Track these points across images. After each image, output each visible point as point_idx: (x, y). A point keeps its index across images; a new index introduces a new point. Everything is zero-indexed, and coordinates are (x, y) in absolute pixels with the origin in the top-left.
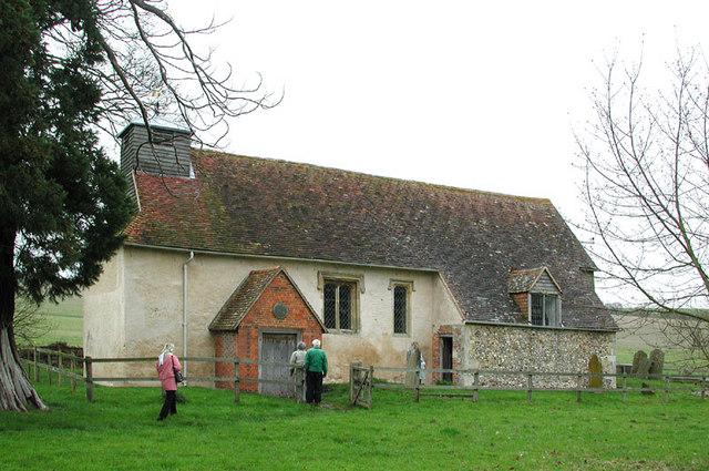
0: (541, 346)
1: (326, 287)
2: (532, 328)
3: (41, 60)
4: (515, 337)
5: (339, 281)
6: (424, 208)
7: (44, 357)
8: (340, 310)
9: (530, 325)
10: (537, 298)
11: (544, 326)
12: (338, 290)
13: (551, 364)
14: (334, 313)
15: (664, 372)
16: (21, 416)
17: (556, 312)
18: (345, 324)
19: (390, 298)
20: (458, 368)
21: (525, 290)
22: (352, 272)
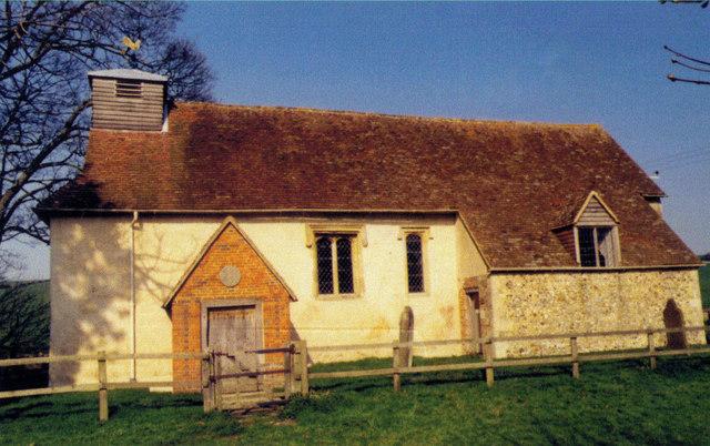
0: (596, 293)
1: (319, 243)
2: (583, 272)
3: (100, 248)
4: (563, 283)
5: (334, 234)
6: (447, 144)
7: (596, 371)
8: (335, 272)
9: (580, 268)
10: (586, 232)
11: (598, 267)
12: (334, 247)
13: (613, 317)
14: (331, 273)
15: (687, 325)
16: (16, 412)
17: (611, 248)
18: (347, 285)
19: (400, 252)
20: (687, 325)
21: (568, 223)
22: (350, 222)
